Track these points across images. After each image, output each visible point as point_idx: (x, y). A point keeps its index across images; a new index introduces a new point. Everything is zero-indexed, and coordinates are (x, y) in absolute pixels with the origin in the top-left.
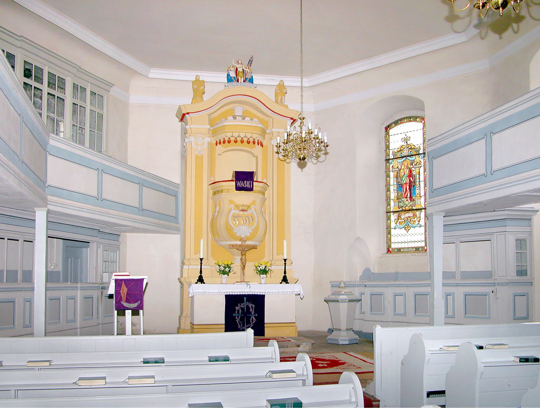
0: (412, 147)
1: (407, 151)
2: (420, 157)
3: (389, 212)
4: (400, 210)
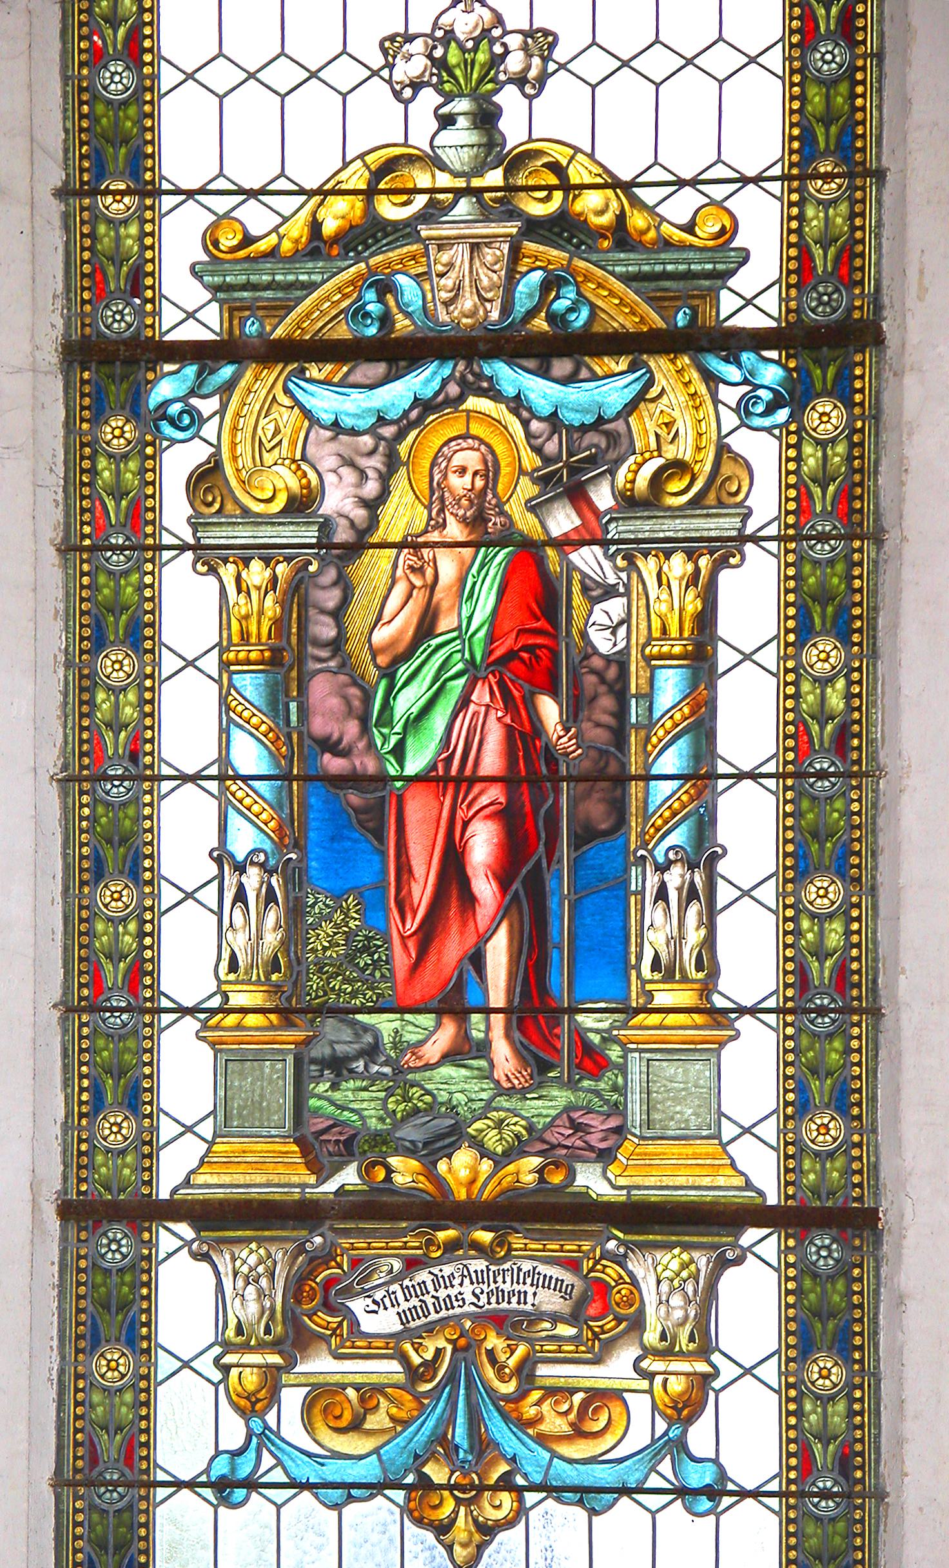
0: (589, 202)
1: (489, 255)
2: (730, 395)
3: (114, 1212)
4: (331, 1186)
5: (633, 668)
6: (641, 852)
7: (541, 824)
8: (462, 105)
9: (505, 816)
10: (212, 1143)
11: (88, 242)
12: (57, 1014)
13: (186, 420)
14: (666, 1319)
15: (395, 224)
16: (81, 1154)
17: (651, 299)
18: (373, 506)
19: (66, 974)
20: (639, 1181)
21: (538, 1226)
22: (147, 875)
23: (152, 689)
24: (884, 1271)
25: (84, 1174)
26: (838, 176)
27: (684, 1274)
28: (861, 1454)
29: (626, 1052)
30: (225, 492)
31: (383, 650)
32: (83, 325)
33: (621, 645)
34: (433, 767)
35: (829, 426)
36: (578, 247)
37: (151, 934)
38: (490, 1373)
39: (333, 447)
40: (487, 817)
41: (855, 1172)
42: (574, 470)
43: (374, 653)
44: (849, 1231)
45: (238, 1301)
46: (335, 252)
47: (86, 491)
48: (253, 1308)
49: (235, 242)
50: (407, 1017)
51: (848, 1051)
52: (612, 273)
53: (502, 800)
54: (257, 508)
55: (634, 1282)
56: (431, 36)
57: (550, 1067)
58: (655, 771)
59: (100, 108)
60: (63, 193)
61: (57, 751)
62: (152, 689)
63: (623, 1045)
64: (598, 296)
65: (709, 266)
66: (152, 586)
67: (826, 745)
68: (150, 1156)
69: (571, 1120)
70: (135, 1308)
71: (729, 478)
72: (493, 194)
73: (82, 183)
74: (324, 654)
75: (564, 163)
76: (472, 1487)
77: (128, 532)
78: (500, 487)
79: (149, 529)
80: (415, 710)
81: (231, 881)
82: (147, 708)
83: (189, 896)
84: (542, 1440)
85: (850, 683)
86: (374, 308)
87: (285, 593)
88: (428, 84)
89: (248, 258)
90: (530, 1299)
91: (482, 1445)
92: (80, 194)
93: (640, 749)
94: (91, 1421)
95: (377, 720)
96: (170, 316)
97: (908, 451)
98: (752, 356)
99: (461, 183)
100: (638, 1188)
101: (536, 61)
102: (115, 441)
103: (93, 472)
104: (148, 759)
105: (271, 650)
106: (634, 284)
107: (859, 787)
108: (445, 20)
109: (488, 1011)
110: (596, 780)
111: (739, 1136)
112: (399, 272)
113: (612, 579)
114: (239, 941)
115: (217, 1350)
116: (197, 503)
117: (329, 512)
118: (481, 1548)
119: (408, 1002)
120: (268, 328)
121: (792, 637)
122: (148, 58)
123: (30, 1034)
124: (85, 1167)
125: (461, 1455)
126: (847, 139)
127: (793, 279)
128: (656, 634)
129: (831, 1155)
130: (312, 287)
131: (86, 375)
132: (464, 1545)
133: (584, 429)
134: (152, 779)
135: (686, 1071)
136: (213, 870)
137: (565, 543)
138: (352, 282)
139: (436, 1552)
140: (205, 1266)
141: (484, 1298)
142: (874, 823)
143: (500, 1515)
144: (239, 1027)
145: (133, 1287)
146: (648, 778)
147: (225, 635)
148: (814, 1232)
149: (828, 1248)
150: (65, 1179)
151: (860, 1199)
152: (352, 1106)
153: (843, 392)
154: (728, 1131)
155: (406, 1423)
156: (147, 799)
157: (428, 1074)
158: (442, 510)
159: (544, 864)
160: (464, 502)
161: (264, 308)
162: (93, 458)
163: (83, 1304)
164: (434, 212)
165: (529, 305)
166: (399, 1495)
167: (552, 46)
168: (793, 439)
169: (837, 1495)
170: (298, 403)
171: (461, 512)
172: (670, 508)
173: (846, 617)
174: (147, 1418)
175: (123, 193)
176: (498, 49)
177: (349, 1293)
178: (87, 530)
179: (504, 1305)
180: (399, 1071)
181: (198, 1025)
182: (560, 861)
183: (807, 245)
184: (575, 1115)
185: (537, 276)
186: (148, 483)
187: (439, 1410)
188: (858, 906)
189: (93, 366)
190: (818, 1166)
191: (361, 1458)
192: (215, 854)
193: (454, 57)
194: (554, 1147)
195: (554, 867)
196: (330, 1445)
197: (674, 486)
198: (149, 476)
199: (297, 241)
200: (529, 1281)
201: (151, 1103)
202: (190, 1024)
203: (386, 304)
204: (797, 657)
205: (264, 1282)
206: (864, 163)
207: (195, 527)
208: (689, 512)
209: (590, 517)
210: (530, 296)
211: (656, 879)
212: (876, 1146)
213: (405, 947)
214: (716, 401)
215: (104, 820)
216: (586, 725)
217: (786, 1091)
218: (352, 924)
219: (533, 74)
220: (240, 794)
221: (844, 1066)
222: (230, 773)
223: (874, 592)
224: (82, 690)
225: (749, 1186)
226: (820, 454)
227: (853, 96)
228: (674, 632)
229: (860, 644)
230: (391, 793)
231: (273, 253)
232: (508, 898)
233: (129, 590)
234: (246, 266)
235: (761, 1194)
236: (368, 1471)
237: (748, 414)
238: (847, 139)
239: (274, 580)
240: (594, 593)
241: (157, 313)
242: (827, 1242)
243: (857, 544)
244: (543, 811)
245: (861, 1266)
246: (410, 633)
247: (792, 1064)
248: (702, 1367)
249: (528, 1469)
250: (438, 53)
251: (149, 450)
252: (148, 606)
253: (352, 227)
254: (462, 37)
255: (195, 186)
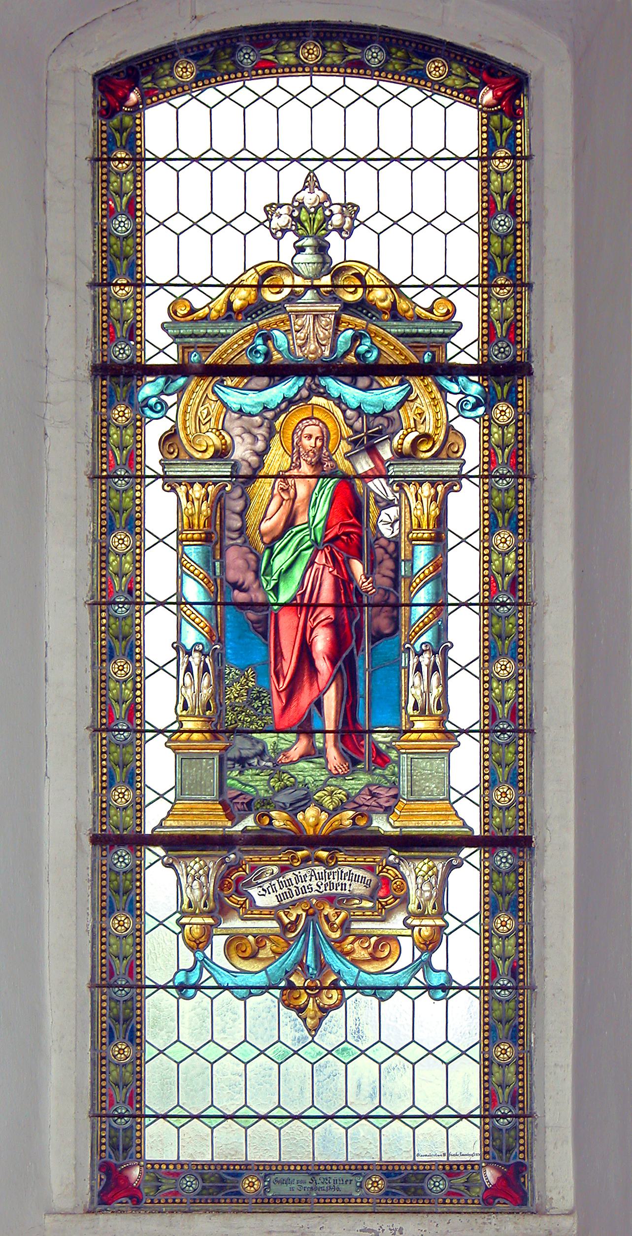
0: (378, 294)
2: (453, 399)
4: (239, 827)
5: (403, 545)
6: (407, 646)
7: (353, 630)
8: (308, 242)
9: (335, 626)
10: (174, 804)
11: (105, 311)
12: (88, 733)
13: (159, 407)
14: (421, 897)
15: (272, 303)
16: (102, 809)
17: (411, 347)
18: (261, 455)
19: (94, 710)
20: (406, 823)
21: (352, 848)
22: (138, 656)
23: (140, 554)
24: (534, 869)
25: (104, 820)
26: (508, 285)
27: (430, 873)
28: (523, 966)
29: (399, 754)
30: (180, 446)
31: (266, 534)
32: (103, 356)
33: (396, 532)
34: (295, 598)
35: (505, 417)
36: (371, 318)
37: (140, 689)
38: (326, 927)
39: (239, 422)
40: (323, 626)
41: (520, 817)
42: (370, 438)
43: (262, 536)
44: (517, 848)
45: (189, 890)
46: (240, 318)
47: (104, 446)
48: (197, 893)
49: (186, 312)
50: (281, 735)
51: (517, 753)
52: (389, 333)
53: (332, 616)
54: (198, 455)
55: (404, 878)
56: (292, 205)
57: (359, 762)
58: (414, 602)
59: (113, 240)
60: (93, 285)
61: (88, 588)
62: (140, 554)
63: (398, 750)
64: (382, 344)
65: (441, 331)
66: (140, 498)
67: (505, 588)
68: (140, 810)
69: (370, 791)
70: (133, 893)
71: (452, 444)
72: (326, 289)
73: (103, 280)
74: (235, 535)
75: (363, 273)
76: (317, 987)
77: (127, 468)
78: (330, 446)
79: (138, 467)
80: (284, 567)
81: (184, 660)
82: (137, 565)
83: (161, 668)
84: (354, 962)
85: (517, 555)
86: (261, 348)
87: (213, 502)
88: (290, 230)
89: (192, 320)
90: (348, 887)
91: (322, 965)
92: (102, 285)
93: (407, 589)
94: (110, 953)
95: (264, 572)
96: (150, 351)
97: (546, 432)
98: (464, 379)
99: (308, 283)
100: (406, 827)
101: (348, 220)
102: (120, 419)
103: (108, 435)
104: (138, 593)
105: (205, 533)
106: (401, 339)
107: (522, 611)
108: (299, 197)
109: (324, 732)
110: (383, 606)
111: (460, 799)
112: (274, 329)
113: (391, 497)
114: (188, 694)
115: (178, 916)
116: (165, 453)
117: (237, 458)
118: (321, 1020)
119: (281, 727)
120: (204, 358)
121: (487, 530)
122: (139, 214)
123: (74, 743)
124: (105, 816)
125: (311, 970)
126: (512, 266)
127: (486, 339)
128: (415, 527)
129: (508, 808)
130: (228, 336)
131: (104, 383)
132: (312, 1018)
133: (375, 415)
134: (483, 604)
135: (431, 764)
136: (174, 654)
137: (365, 477)
138: (249, 334)
139: (297, 1022)
140: (171, 871)
141: (323, 887)
142: (530, 630)
143: (331, 1002)
144: (188, 740)
145: (132, 881)
146: (411, 605)
147: (180, 525)
148: (499, 849)
149: (506, 857)
150: (94, 823)
151: (523, 831)
152: (251, 784)
153: (512, 399)
154: (454, 796)
155: (281, 954)
156: (138, 614)
157: (292, 766)
158: (299, 458)
159: (355, 652)
160: (311, 454)
161: (202, 347)
162: (107, 428)
163: (104, 890)
164: (293, 298)
165: (346, 348)
166: (277, 992)
167: (357, 212)
168: (486, 424)
169: (510, 988)
170: (219, 398)
171: (309, 459)
172: (421, 459)
173: (515, 519)
174: (140, 951)
175: (125, 285)
176: (327, 213)
177: (249, 885)
178: (104, 467)
179: (334, 891)
180: (276, 765)
181: (166, 739)
182: (364, 650)
183: (492, 322)
184: (372, 788)
185: (350, 333)
186: (138, 442)
187: (298, 947)
188: (522, 675)
189: (108, 378)
190: (501, 815)
191: (256, 973)
192: (175, 645)
193: (304, 216)
194: (360, 806)
195: (360, 653)
196: (239, 966)
197: (424, 447)
198: (139, 438)
199: (219, 312)
200: (347, 878)
201: (140, 782)
202: (162, 739)
203: (268, 347)
204: (490, 540)
205: (203, 879)
206: (521, 279)
207: (163, 466)
208: (432, 461)
209: (379, 463)
210: (346, 343)
211: (415, 660)
212: (531, 803)
213: (279, 697)
214: (446, 402)
215: (114, 626)
216: (377, 576)
217: (485, 774)
218: (250, 684)
219: (346, 226)
220: (188, 612)
221: (515, 761)
222: (183, 601)
223: (529, 507)
224: (102, 554)
225: (465, 825)
226: (500, 432)
227: (515, 244)
228: (425, 527)
229: (523, 534)
230: (271, 613)
231: (206, 318)
232: (335, 670)
233: (128, 499)
234: (191, 324)
235: (471, 829)
236: (260, 979)
237: (462, 409)
238: (512, 266)
239: (207, 494)
240: (381, 504)
241: (143, 349)
242: (506, 854)
243: (520, 480)
244: (354, 623)
245: (523, 867)
246: (282, 524)
247: (487, 760)
248: (439, 922)
249: (347, 978)
250: (296, 214)
251: (138, 424)
252: (138, 509)
253: (249, 305)
254: (308, 206)
255: (164, 282)
